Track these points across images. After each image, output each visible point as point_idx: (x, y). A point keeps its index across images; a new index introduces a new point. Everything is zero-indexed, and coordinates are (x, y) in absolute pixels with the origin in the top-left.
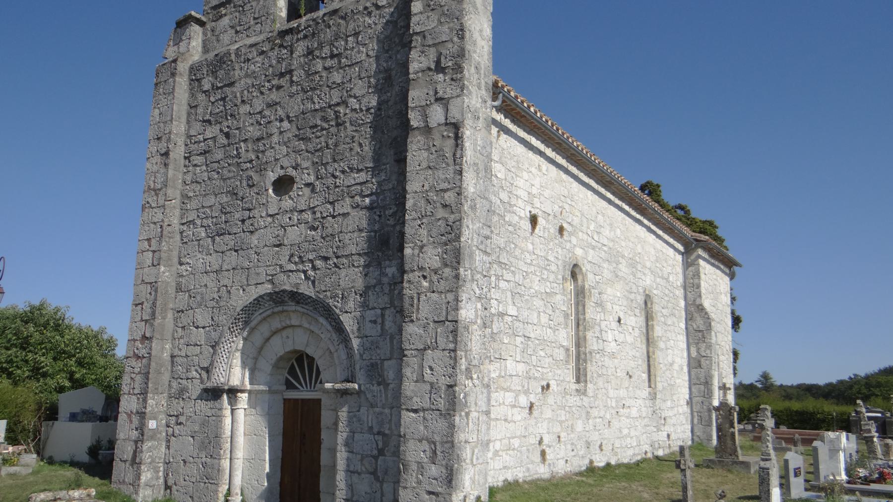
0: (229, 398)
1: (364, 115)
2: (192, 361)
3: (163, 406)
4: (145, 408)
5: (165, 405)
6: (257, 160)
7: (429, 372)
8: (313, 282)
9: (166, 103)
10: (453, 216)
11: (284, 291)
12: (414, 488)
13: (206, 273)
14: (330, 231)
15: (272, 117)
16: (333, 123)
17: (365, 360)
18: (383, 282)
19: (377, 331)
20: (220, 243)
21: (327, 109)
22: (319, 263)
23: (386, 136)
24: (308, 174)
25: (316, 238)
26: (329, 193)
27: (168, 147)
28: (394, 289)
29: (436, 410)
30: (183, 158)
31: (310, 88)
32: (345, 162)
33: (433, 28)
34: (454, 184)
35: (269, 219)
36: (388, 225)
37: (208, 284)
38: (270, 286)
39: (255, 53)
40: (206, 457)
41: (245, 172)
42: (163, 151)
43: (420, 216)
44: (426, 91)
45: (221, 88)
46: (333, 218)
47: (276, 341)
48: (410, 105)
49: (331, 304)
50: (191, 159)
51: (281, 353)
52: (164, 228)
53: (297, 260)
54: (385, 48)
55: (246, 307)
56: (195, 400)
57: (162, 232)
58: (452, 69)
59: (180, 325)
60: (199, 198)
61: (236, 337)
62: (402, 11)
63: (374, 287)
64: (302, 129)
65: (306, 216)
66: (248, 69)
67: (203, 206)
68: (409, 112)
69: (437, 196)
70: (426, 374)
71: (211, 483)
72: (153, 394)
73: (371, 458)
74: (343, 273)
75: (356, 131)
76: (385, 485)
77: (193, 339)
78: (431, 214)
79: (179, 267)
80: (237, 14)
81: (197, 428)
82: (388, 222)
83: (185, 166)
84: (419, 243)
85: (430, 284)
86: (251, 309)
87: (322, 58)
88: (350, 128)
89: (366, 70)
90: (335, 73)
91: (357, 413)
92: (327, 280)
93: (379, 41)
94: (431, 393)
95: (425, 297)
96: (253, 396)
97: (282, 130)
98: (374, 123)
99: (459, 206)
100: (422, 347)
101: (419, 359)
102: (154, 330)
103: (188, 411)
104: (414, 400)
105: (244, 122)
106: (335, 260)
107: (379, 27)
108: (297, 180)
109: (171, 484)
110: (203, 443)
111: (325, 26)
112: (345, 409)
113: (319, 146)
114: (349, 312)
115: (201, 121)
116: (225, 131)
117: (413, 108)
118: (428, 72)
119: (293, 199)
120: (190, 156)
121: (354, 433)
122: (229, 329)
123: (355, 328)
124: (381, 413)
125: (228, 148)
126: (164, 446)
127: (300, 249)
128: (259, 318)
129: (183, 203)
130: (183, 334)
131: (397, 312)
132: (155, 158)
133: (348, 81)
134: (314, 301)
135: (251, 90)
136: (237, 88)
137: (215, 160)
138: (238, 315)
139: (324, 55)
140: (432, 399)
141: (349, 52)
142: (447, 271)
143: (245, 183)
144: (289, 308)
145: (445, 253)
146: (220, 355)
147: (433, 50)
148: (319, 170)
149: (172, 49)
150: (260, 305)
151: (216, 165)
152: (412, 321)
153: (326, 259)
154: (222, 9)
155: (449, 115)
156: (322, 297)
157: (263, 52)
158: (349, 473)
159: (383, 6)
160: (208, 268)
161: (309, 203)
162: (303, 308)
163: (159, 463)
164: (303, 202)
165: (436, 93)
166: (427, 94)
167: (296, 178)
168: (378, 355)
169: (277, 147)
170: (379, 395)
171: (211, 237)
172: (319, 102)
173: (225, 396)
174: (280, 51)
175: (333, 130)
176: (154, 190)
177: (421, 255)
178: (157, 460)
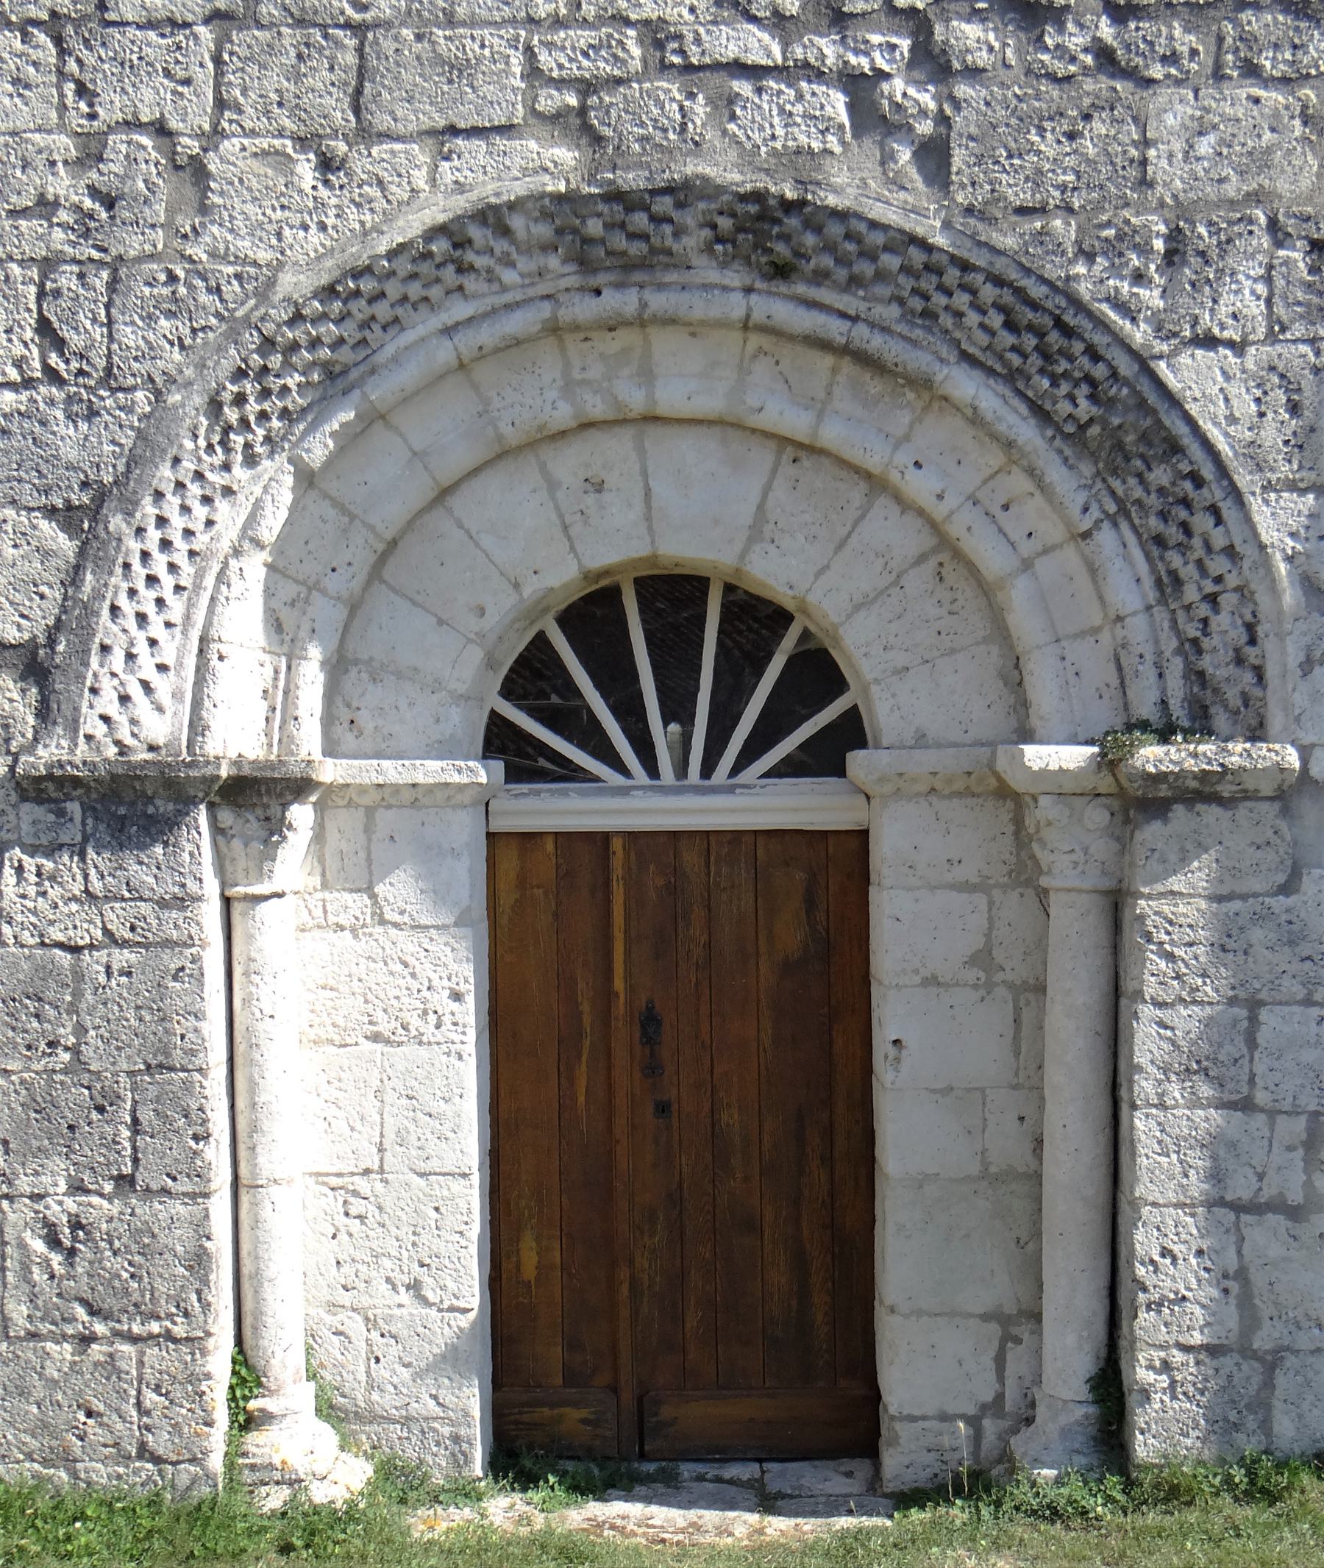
11: (682, 192)
38: (565, 155)
40: (77, 1188)
49: (1084, 289)
55: (357, 274)
61: (251, 460)
86: (393, 289)
91: (1279, 903)
106: (1106, 30)
114: (1230, 344)
121: (1254, 1005)
122: (215, 406)
123: (1271, 435)
128: (444, 353)
138: (297, 318)
144: (698, 306)
156: (1009, 242)
158: (1229, 1216)
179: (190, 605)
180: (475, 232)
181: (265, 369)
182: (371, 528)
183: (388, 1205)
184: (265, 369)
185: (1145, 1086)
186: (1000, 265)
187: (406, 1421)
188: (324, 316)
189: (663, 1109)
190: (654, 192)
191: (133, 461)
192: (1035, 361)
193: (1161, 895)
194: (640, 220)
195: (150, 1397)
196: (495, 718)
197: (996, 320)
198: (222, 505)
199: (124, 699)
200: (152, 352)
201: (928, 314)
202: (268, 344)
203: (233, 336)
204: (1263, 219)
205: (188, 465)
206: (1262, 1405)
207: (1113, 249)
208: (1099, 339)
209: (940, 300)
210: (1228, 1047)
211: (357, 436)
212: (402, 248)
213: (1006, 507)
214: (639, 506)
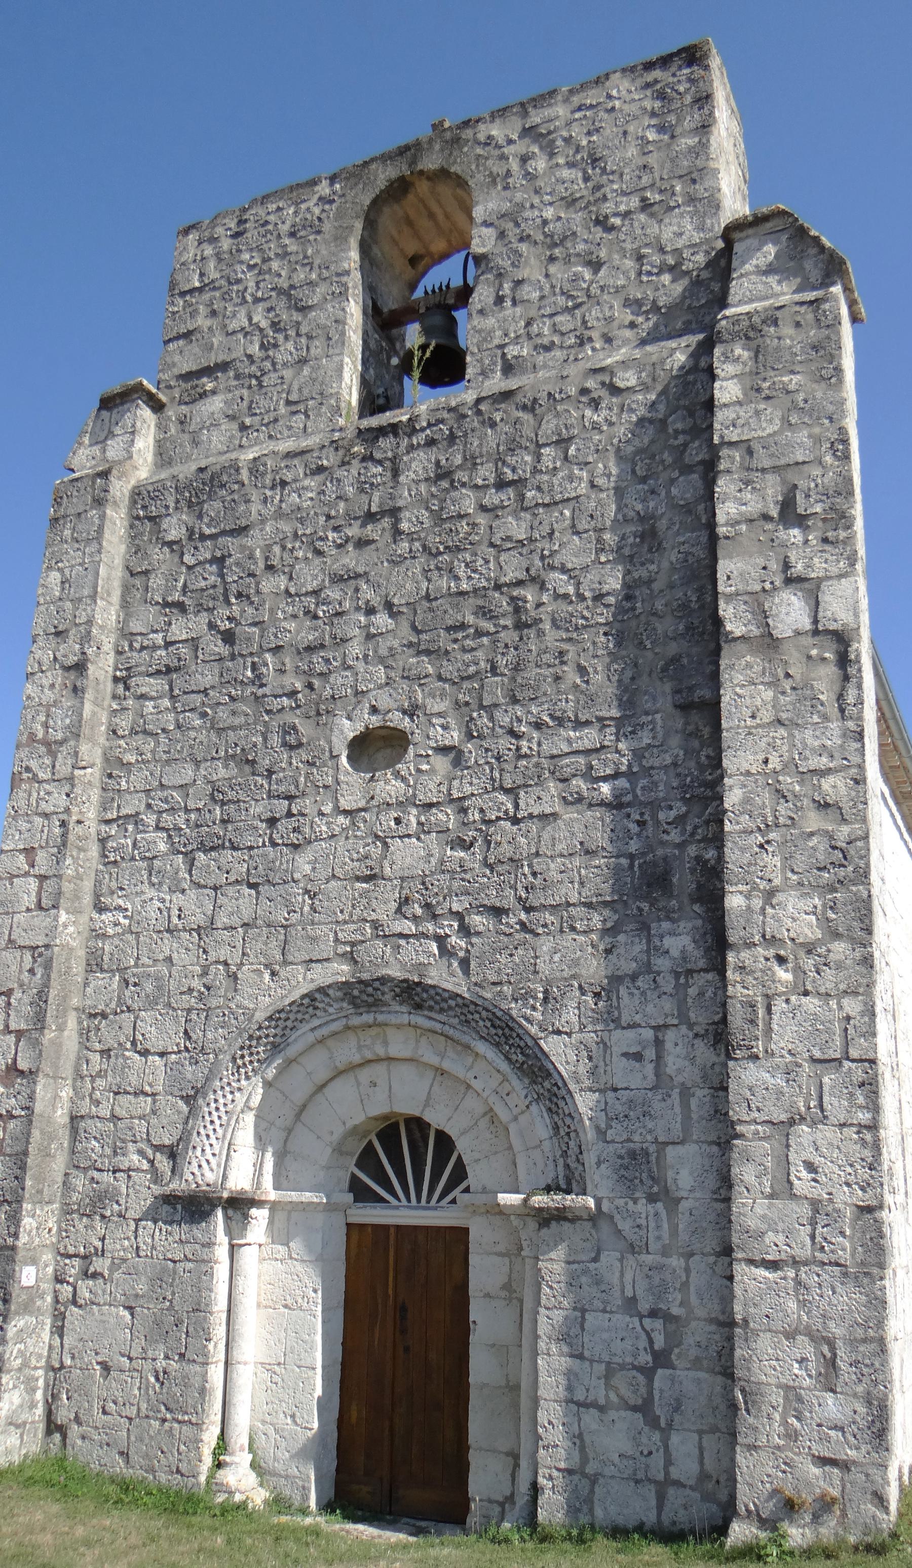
0: (227, 1218)
1: (588, 608)
2: (130, 1129)
3: (50, 1230)
4: (16, 1236)
5: (55, 1230)
6: (307, 691)
7: (804, 1174)
8: (465, 963)
9: (79, 560)
10: (845, 829)
11: (383, 980)
12: (778, 1448)
13: (169, 931)
14: (506, 850)
15: (347, 605)
16: (509, 622)
17: (613, 1141)
18: (656, 968)
19: (645, 1078)
20: (209, 866)
21: (490, 593)
22: (477, 921)
23: (649, 654)
24: (445, 727)
25: (468, 865)
26: (502, 770)
27: (84, 653)
28: (687, 985)
29: (830, 1264)
30: (110, 679)
31: (446, 548)
32: (542, 703)
33: (770, 435)
34: (845, 759)
35: (342, 820)
36: (663, 843)
37: (175, 956)
38: (345, 968)
39: (301, 472)
40: (167, 1357)
41: (278, 716)
42: (72, 659)
43: (762, 826)
44: (761, 562)
45: (212, 537)
46: (513, 824)
47: (343, 1090)
48: (721, 588)
49: (514, 1013)
50: (132, 682)
51: (359, 1118)
52: (71, 827)
53: (419, 911)
54: (639, 473)
55: (279, 1012)
56: (137, 1221)
57: (64, 835)
58: (824, 520)
59: (98, 1047)
60: (151, 766)
61: (248, 1078)
62: (678, 399)
63: (634, 977)
64: (426, 632)
65: (444, 818)
66: (281, 501)
67: (161, 785)
68: (722, 604)
69: (801, 783)
70: (799, 1179)
71: (179, 1422)
72: (34, 1203)
73: (634, 1373)
74: (545, 945)
75: (570, 640)
76: (675, 1439)
77: (134, 1080)
78: (789, 822)
79: (95, 916)
80: (245, 392)
81: (141, 1287)
82: (665, 837)
83: (115, 697)
84: (763, 885)
85: (795, 977)
86: (292, 1016)
87: (476, 487)
88: (552, 636)
89: (592, 516)
90: (510, 519)
91: (592, 1266)
92: (503, 959)
93: (620, 457)
94: (813, 1223)
95: (784, 1005)
96: (281, 1216)
97: (373, 630)
98: (617, 625)
99: (861, 806)
100: (784, 1117)
101: (776, 1144)
102: (40, 1054)
103: (118, 1247)
104: (767, 1241)
105: (272, 611)
106: (523, 916)
107: (621, 431)
108: (417, 737)
109: (65, 1421)
110: (158, 1323)
111: (483, 423)
112: (559, 1253)
113: (472, 669)
114: (566, 1033)
115: (157, 603)
116: (222, 628)
117: (729, 597)
118: (762, 522)
119: (404, 779)
120: (129, 677)
121: (583, 1311)
122: (234, 1059)
123: (584, 1067)
124: (660, 1268)
125: (230, 664)
126: (48, 1328)
127: (427, 889)
128: (311, 1038)
129: (110, 776)
130: (104, 1066)
131: (696, 1035)
132: (49, 674)
133: (544, 537)
134: (466, 1005)
135: (289, 546)
136: (255, 541)
137: (195, 689)
138: (260, 1028)
139: (480, 482)
140: (818, 1239)
141: (546, 478)
142: (840, 949)
143: (275, 740)
144: (393, 1019)
145: (831, 908)
146: (207, 1118)
147: (772, 479)
148: (472, 719)
149: (87, 452)
150: (316, 1008)
151: (198, 699)
152: (756, 1057)
153: (498, 912)
154: (205, 380)
155: (821, 614)
156: (488, 995)
157: (321, 469)
158: (574, 1408)
159: (628, 389)
160: (175, 920)
161: (449, 790)
162: (430, 1018)
163: (36, 1368)
164: (432, 786)
165: (787, 566)
166: (764, 568)
167: (412, 734)
168: (650, 1131)
169: (361, 666)
170: (652, 1225)
171: (185, 854)
172: (470, 578)
173: (219, 1213)
174: (365, 468)
175: (509, 636)
176: (47, 743)
177: (769, 910)
178: (34, 1362)
179: (225, 1131)
180: (317, 996)
181: (250, 1046)
182: (292, 1101)
183: (285, 1377)
184: (250, 1046)
185: (542, 1345)
186: (486, 1004)
187: (287, 1477)
188: (269, 1027)
189: (407, 1349)
190: (373, 980)
191: (207, 1079)
192: (503, 1039)
193: (547, 1260)
194: (370, 990)
195: (182, 1447)
196: (354, 1177)
197: (489, 1024)
198: (237, 1094)
199: (200, 1166)
200: (216, 1041)
201: (466, 1021)
202: (251, 1038)
203: (240, 1035)
204: (576, 985)
205: (225, 1080)
206: (589, 1501)
207: (524, 997)
208: (521, 1031)
209: (470, 1017)
210: (573, 1330)
211: (285, 1068)
212: (293, 1002)
213: (508, 1094)
214: (387, 1092)
